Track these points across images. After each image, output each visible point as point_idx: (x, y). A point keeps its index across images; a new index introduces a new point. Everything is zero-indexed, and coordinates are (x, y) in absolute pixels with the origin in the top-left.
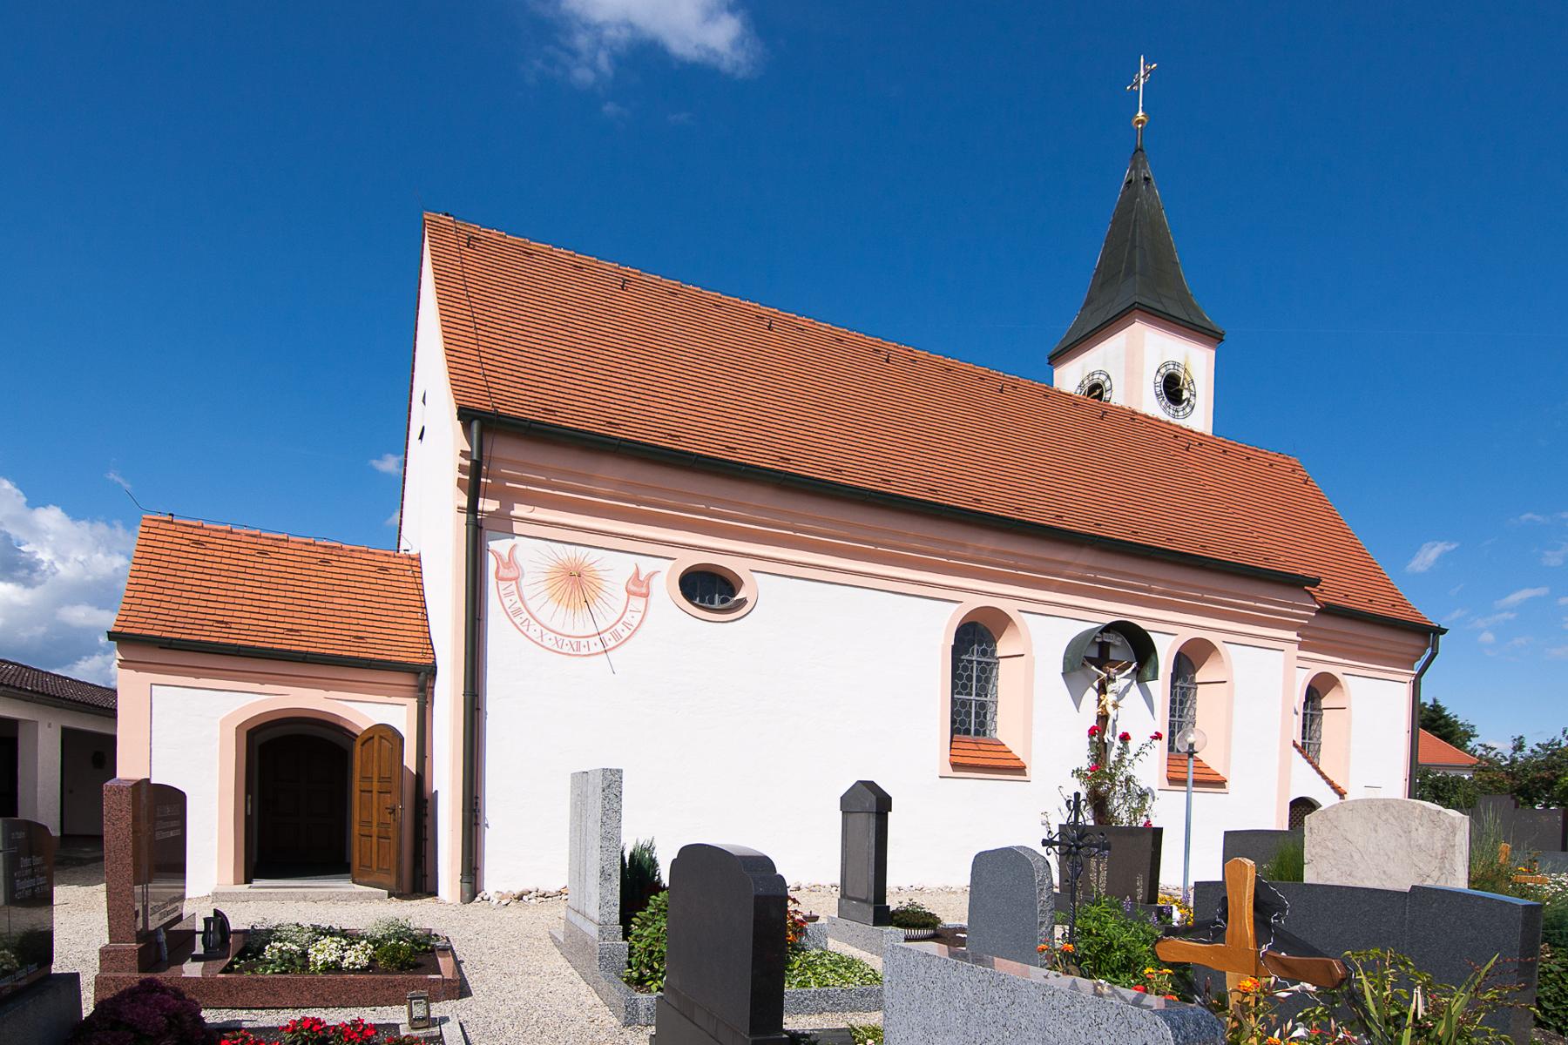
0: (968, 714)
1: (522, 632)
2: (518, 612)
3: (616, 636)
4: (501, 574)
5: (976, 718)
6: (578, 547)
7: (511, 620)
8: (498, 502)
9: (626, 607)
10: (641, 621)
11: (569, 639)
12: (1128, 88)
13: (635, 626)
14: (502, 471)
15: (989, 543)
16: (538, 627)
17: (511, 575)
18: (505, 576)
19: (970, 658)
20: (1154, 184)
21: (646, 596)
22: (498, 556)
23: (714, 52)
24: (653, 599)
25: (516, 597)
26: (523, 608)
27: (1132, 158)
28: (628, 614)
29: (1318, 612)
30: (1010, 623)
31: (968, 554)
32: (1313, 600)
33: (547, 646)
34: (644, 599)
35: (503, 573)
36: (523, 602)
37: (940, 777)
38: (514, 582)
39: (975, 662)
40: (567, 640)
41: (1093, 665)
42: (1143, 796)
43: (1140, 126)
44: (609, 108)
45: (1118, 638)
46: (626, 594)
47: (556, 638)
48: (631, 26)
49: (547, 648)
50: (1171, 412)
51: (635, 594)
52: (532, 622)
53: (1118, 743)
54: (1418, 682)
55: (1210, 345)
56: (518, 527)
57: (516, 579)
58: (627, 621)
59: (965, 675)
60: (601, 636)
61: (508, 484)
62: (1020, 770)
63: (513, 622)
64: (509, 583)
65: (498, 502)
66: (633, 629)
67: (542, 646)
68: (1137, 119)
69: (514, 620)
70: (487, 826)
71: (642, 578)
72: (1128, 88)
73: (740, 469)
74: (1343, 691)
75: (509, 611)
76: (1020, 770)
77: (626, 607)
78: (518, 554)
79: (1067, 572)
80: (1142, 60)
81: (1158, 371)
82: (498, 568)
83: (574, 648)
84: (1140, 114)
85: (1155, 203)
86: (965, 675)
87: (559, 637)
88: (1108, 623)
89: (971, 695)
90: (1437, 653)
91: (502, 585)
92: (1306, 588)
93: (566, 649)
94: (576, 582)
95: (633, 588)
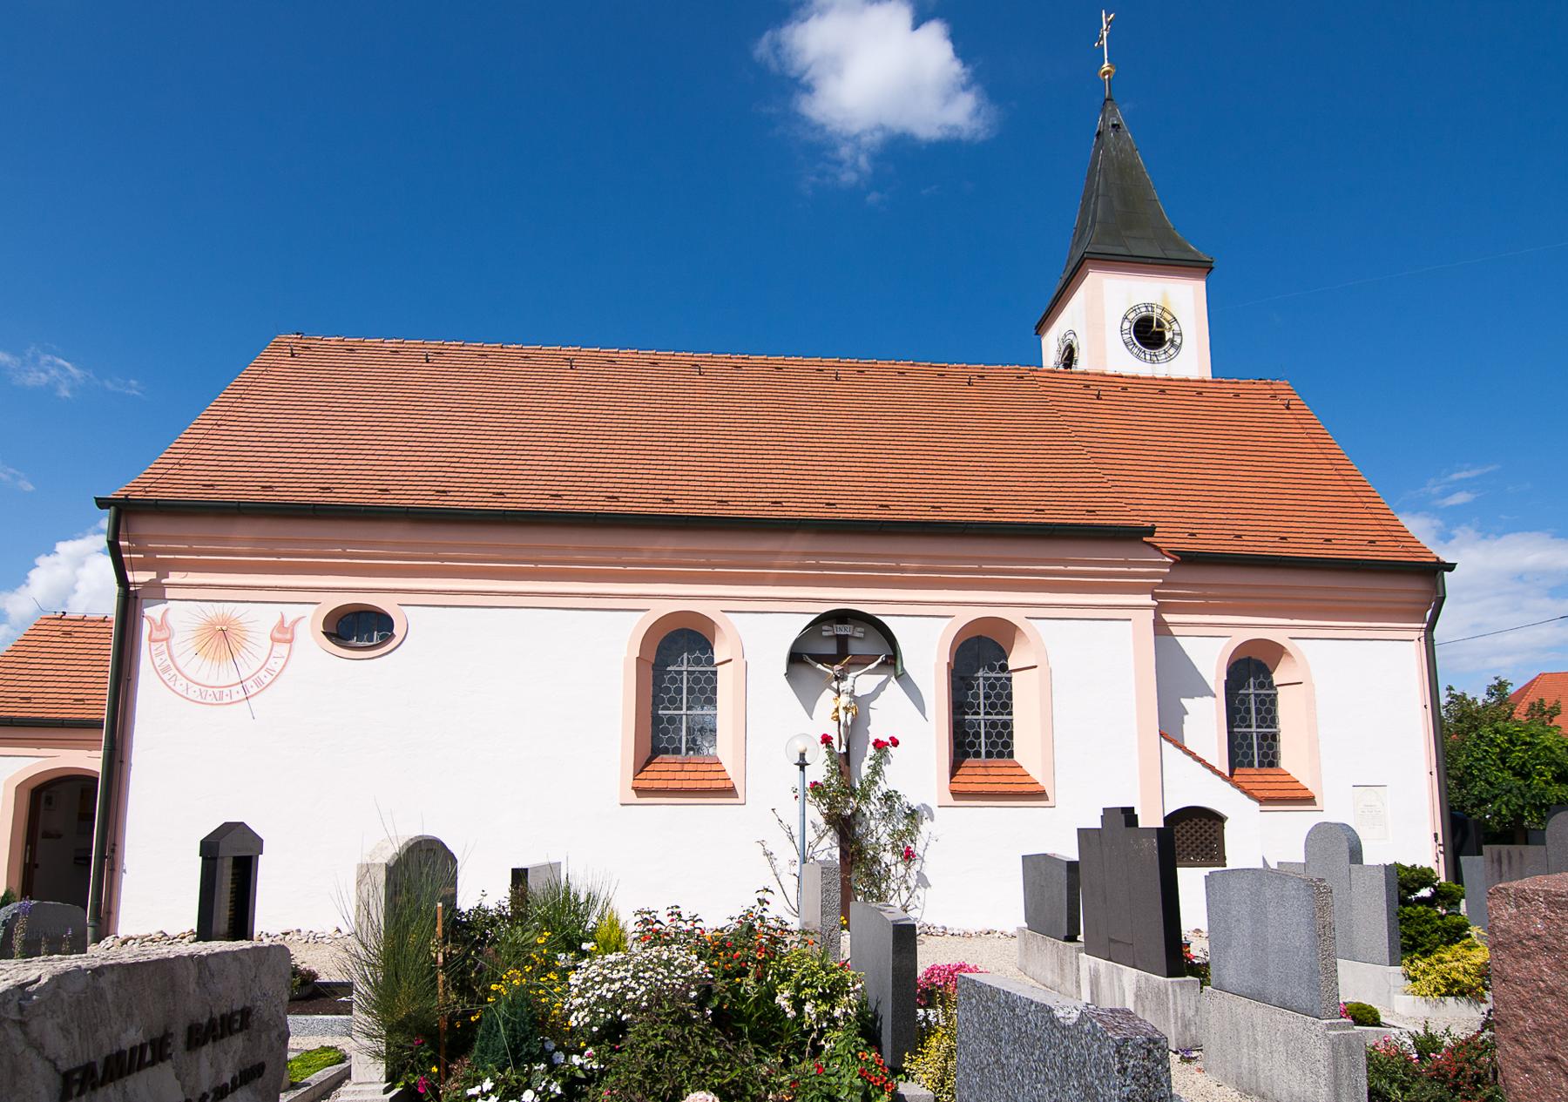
0: (1250, 746)
1: (170, 687)
2: (167, 669)
3: (258, 682)
4: (153, 636)
5: (1258, 749)
6: (225, 604)
7: (160, 677)
8: (155, 573)
9: (270, 654)
10: (284, 666)
11: (212, 689)
12: (1096, 45)
13: (278, 671)
14: (150, 545)
15: (667, 543)
16: (185, 681)
17: (162, 637)
18: (157, 638)
19: (678, 669)
20: (1126, 129)
21: (290, 641)
22: (152, 621)
23: (954, 128)
24: (296, 644)
25: (166, 656)
26: (172, 666)
27: (1102, 110)
28: (271, 660)
29: (1172, 566)
30: (1017, 633)
31: (645, 558)
32: (1159, 553)
33: (192, 698)
34: (289, 645)
35: (156, 635)
36: (172, 660)
37: (622, 804)
38: (165, 643)
39: (685, 673)
40: (210, 691)
41: (819, 663)
42: (913, 815)
43: (1107, 77)
44: (873, 198)
45: (859, 629)
46: (271, 642)
47: (200, 690)
48: (882, 128)
49: (192, 701)
50: (1163, 356)
51: (279, 641)
52: (179, 676)
53: (871, 751)
54: (1429, 638)
55: (1196, 277)
56: (169, 593)
57: (166, 639)
58: (269, 667)
59: (673, 687)
60: (244, 683)
61: (158, 556)
62: (730, 792)
63: (162, 679)
64: (160, 643)
65: (155, 573)
66: (275, 674)
67: (187, 699)
68: (1103, 71)
69: (163, 676)
70: (125, 871)
71: (286, 626)
72: (1096, 45)
73: (360, 510)
74: (1294, 661)
75: (159, 669)
76: (1040, 795)
77: (270, 654)
78: (170, 617)
79: (778, 562)
80: (1104, 15)
81: (1126, 318)
82: (151, 631)
83: (216, 697)
84: (1106, 64)
85: (1127, 147)
86: (673, 687)
87: (203, 689)
88: (823, 611)
89: (979, 714)
90: (1444, 598)
91: (155, 646)
92: (1145, 539)
93: (209, 700)
94: (223, 637)
95: (277, 635)
